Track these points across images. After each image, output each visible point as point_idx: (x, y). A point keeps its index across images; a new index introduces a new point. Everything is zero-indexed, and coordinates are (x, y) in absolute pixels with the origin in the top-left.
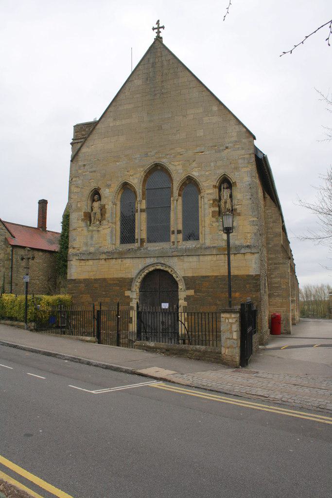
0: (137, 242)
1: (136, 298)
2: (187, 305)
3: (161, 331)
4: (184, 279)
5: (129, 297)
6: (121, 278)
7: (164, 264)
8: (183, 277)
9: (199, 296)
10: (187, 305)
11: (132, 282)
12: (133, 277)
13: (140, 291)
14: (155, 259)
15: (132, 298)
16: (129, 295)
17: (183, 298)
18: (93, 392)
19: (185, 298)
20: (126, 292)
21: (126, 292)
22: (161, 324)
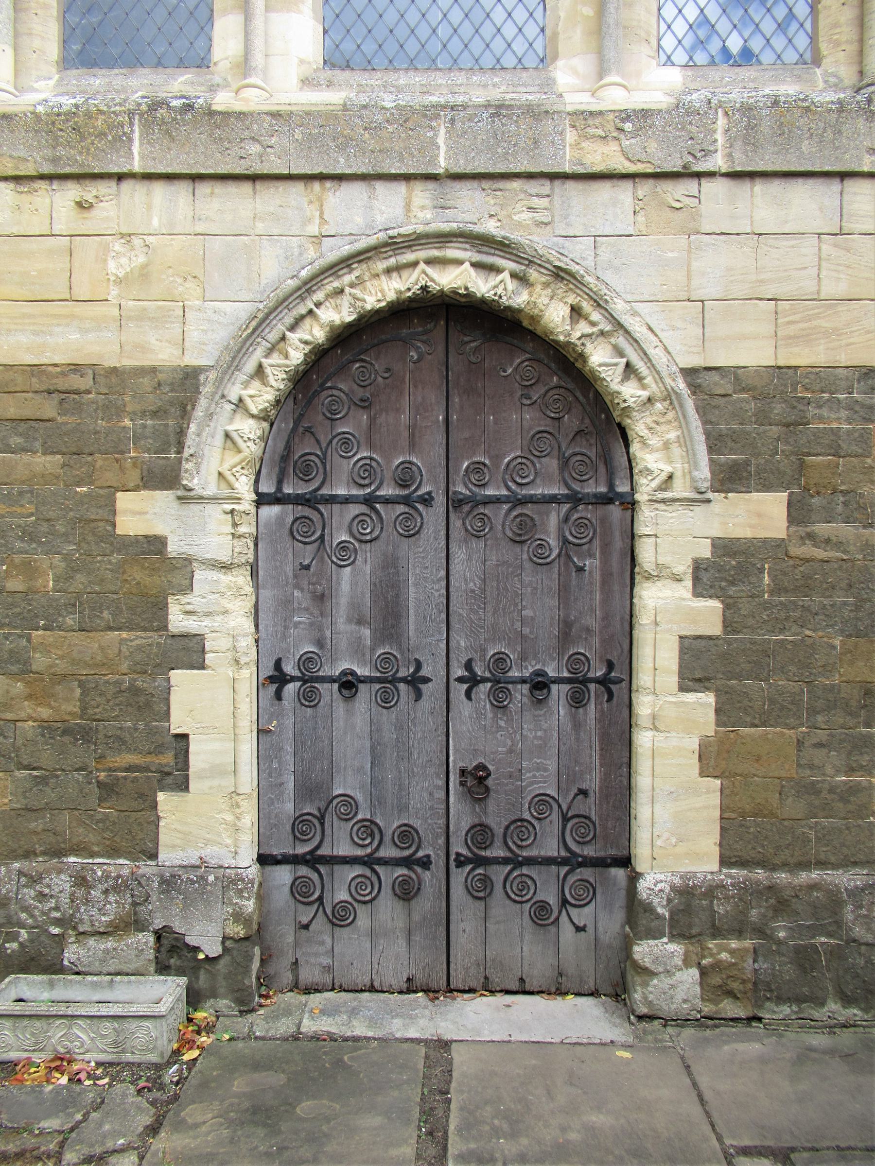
0: (463, 772)
1: (224, 556)
2: (715, 628)
3: (458, 847)
4: (695, 388)
5: (156, 543)
6: (76, 368)
7: (503, 246)
8: (690, 373)
9: (839, 545)
10: (715, 628)
11: (185, 410)
12: (192, 360)
13: (261, 500)
14: (422, 194)
15: (188, 561)
16: (159, 529)
17: (684, 567)
18: (766, 575)
19: (699, 568)
20: (123, 500)
21: (123, 500)
22: (329, 641)
